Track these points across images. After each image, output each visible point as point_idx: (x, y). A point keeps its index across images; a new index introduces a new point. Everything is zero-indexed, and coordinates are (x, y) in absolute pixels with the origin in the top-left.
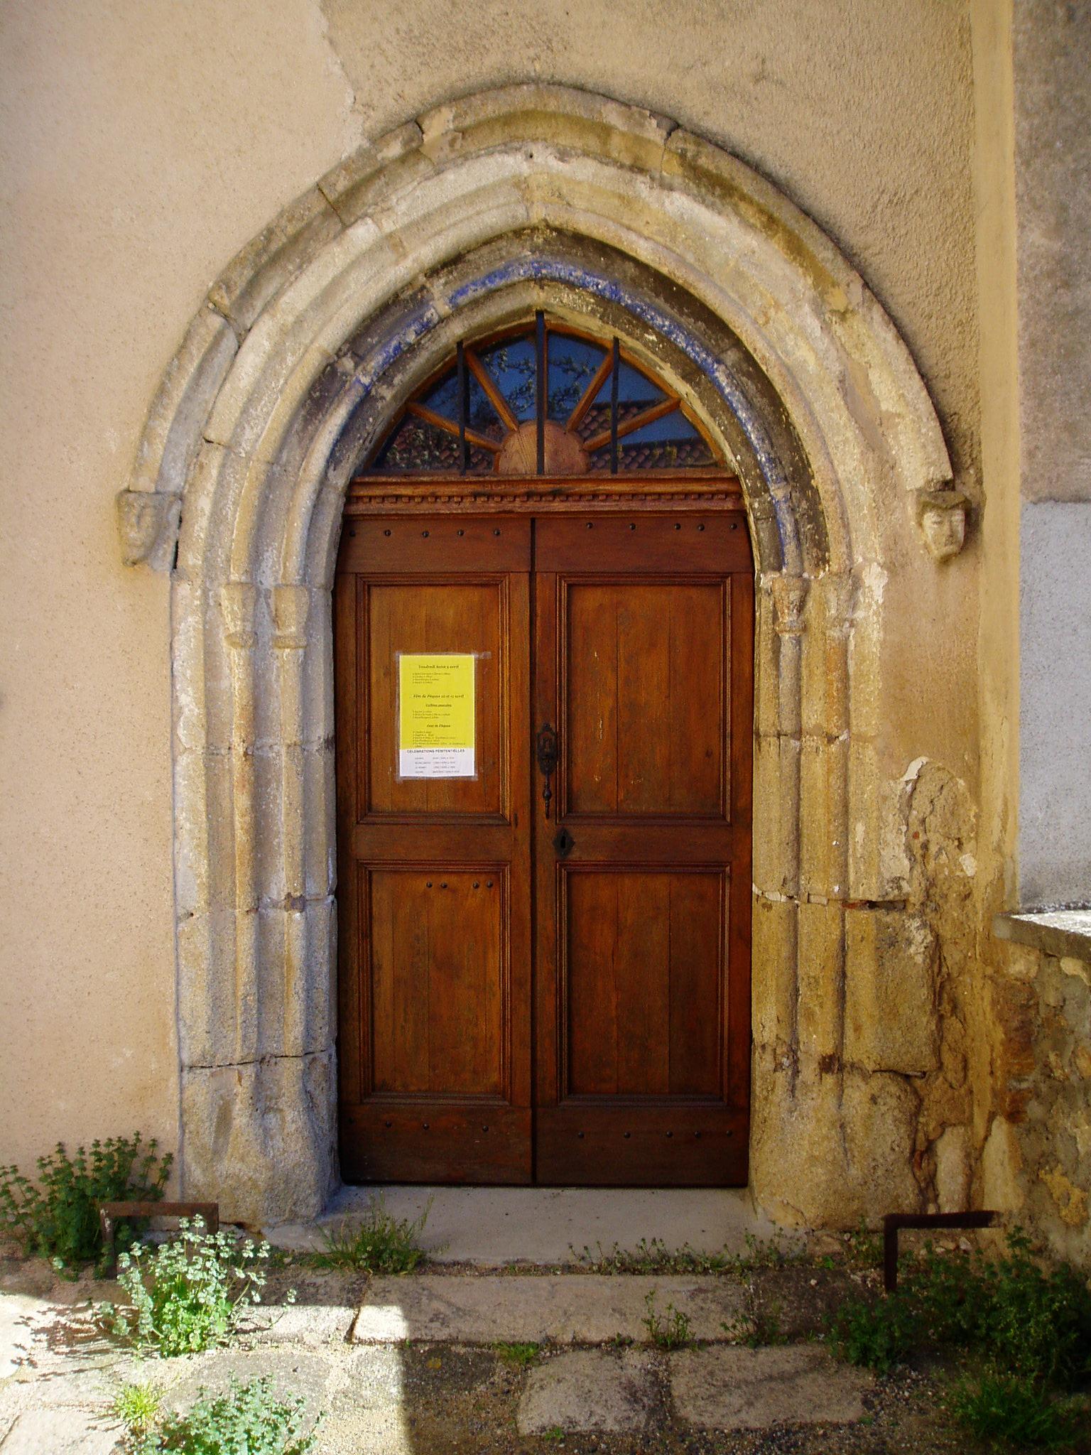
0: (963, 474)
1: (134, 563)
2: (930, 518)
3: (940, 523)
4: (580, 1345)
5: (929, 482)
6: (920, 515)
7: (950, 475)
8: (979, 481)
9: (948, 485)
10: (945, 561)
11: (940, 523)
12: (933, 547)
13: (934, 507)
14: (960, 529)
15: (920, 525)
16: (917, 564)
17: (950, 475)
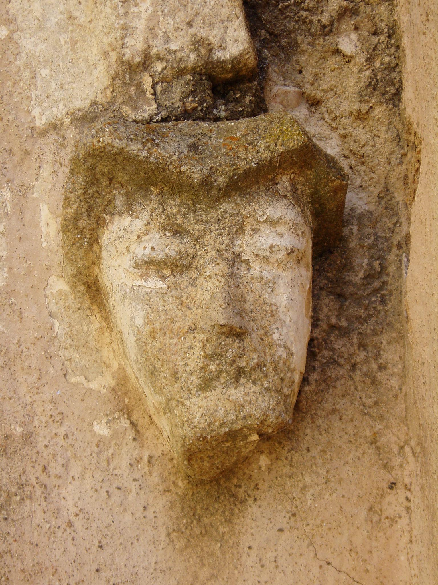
0: (307, 59)
1: (138, 431)
2: (131, 238)
3: (177, 266)
4: (411, 537)
5: (130, 71)
6: (84, 230)
7: (234, 42)
8: (386, 87)
9: (225, 89)
10: (218, 474)
11: (177, 266)
12: (152, 400)
13: (151, 180)
14: (285, 298)
15: (92, 290)
16: (74, 494)
17: (234, 42)
